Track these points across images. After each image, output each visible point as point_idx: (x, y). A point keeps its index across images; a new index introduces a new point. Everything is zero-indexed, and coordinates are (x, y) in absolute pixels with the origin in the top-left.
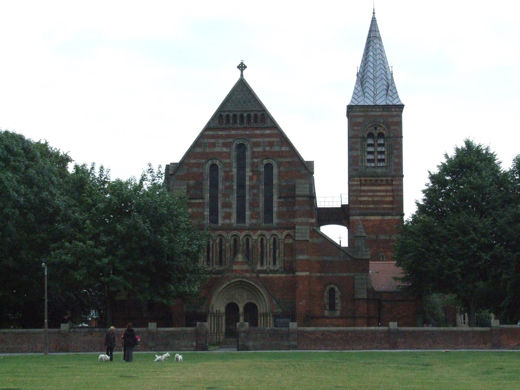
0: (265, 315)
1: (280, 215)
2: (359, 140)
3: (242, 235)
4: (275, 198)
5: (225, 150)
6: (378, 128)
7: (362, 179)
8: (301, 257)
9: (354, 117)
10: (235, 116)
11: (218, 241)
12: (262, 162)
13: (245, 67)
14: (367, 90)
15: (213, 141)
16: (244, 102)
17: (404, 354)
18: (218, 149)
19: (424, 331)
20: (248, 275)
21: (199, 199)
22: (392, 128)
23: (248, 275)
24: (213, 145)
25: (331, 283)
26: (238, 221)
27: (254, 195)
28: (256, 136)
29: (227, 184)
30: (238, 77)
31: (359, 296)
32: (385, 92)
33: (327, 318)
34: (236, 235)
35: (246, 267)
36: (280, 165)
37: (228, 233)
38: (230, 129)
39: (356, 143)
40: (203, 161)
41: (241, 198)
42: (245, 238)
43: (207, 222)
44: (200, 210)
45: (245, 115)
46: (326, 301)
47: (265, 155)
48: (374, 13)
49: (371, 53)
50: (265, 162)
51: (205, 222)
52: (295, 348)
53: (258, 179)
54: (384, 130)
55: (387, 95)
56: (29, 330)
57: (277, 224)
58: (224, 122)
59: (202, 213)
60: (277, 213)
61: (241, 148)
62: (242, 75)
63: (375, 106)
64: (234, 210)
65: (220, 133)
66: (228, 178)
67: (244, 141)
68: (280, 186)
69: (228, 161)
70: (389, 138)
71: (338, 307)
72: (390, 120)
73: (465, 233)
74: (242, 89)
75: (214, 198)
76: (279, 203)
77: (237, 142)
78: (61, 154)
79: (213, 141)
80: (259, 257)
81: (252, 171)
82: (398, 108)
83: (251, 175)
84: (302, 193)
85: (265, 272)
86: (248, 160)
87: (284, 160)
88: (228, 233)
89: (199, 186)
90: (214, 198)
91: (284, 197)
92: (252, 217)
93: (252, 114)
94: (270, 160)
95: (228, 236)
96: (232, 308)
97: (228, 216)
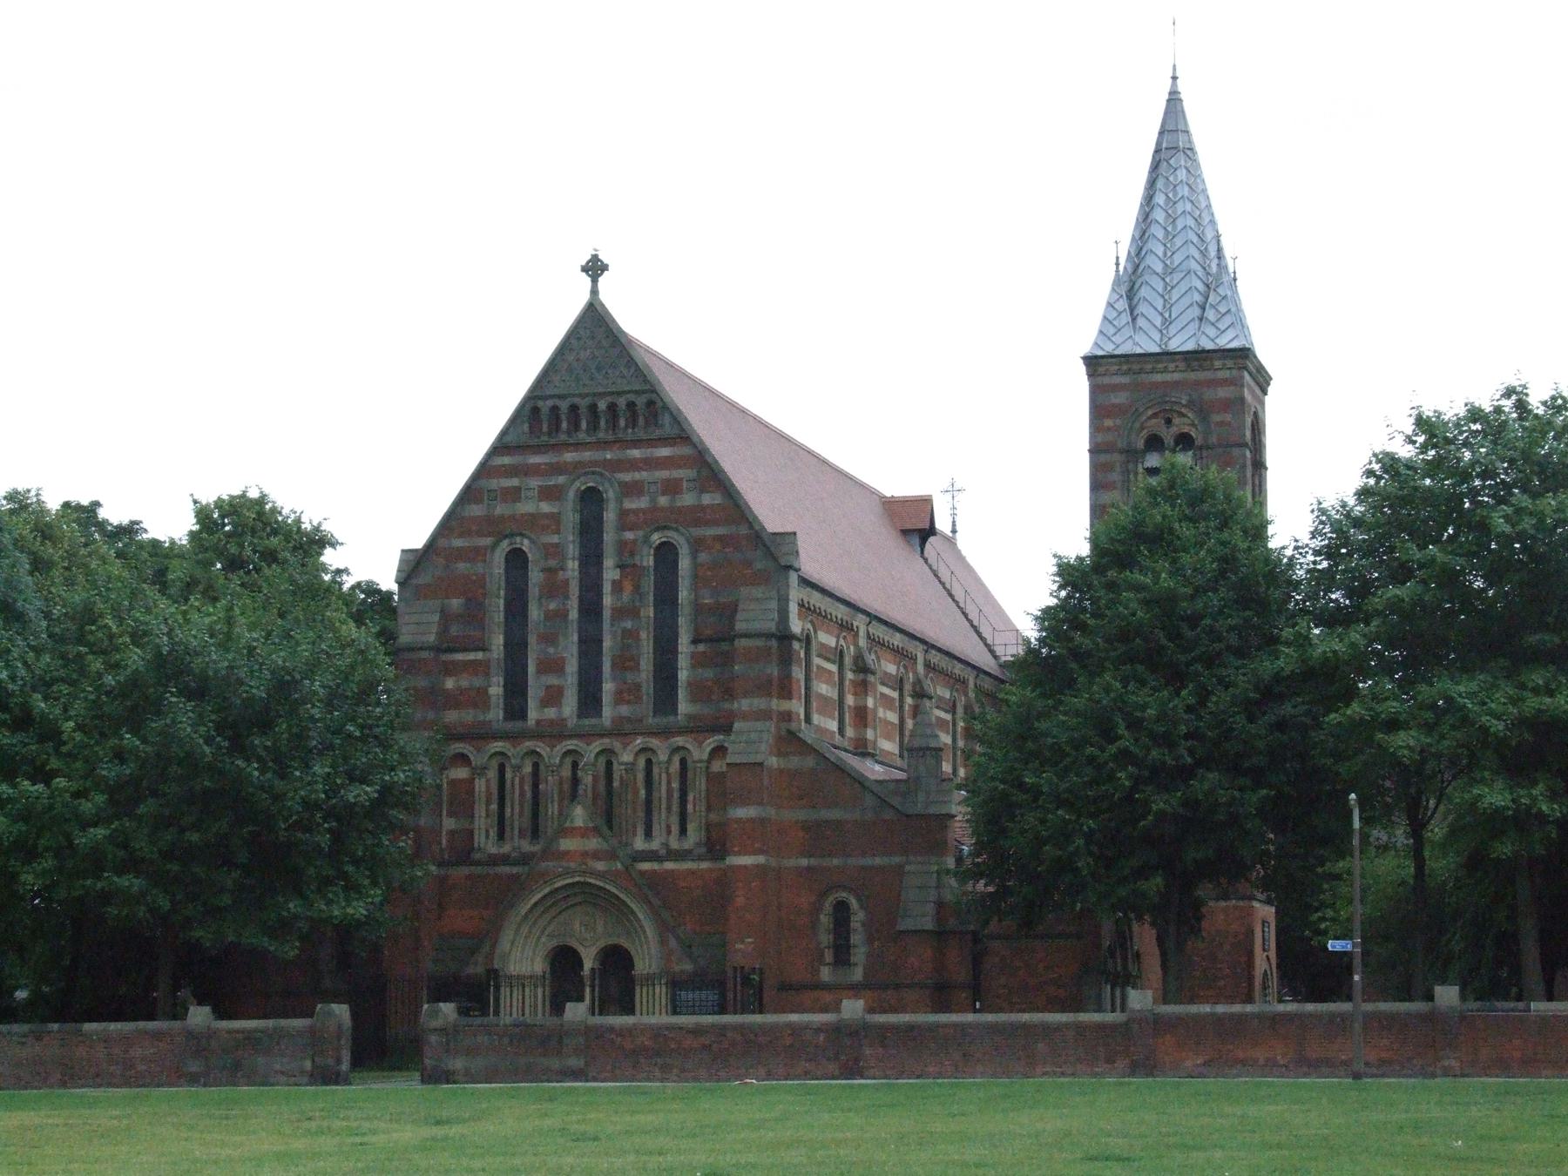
0: (650, 980)
1: (699, 691)
2: (1117, 457)
3: (591, 750)
5: (546, 507)
6: (1176, 421)
8: (742, 813)
10: (574, 408)
11: (528, 769)
12: (646, 539)
13: (604, 268)
14: (1142, 308)
15: (515, 482)
16: (599, 369)
17: (877, 1088)
18: (526, 507)
20: (600, 866)
22: (1216, 418)
23: (600, 866)
24: (514, 495)
28: (633, 465)
29: (552, 606)
30: (584, 298)
31: (906, 924)
32: (1197, 311)
34: (502, 754)
35: (593, 843)
36: (697, 545)
40: (488, 541)
42: (602, 760)
43: (496, 714)
44: (478, 682)
45: (602, 405)
46: (825, 939)
47: (655, 520)
48: (1174, 78)
49: (1160, 199)
50: (656, 538)
51: (491, 716)
52: (577, 1075)
54: (1193, 425)
55: (1201, 319)
56: (283, 1022)
57: (690, 717)
58: (545, 429)
59: (483, 692)
60: (689, 684)
61: (591, 499)
62: (594, 292)
63: (1167, 355)
66: (554, 589)
68: (698, 608)
69: (555, 539)
70: (1208, 448)
71: (859, 954)
72: (1209, 394)
73: (1109, 735)
74: (595, 333)
75: (516, 649)
76: (693, 656)
77: (581, 484)
78: (306, 526)
79: (515, 482)
80: (641, 814)
81: (621, 567)
82: (1127, 362)
83: (617, 577)
84: (756, 626)
85: (652, 856)
86: (609, 537)
87: (711, 532)
89: (475, 613)
90: (516, 649)
91: (710, 640)
92: (619, 698)
93: (621, 402)
94: (671, 533)
95: (552, 754)
96: (564, 960)
97: (554, 699)
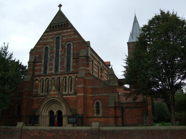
1: (74, 67)
4: (72, 60)
5: (51, 40)
9: (129, 46)
13: (62, 6)
15: (47, 37)
18: (48, 41)
19: (123, 131)
21: (40, 63)
23: (56, 96)
24: (47, 39)
25: (97, 99)
26: (55, 72)
28: (64, 33)
31: (110, 106)
33: (95, 117)
35: (56, 92)
36: (74, 44)
37: (50, 77)
38: (53, 31)
41: (57, 61)
44: (40, 68)
46: (95, 109)
48: (135, 15)
49: (135, 26)
50: (68, 43)
53: (64, 52)
60: (72, 66)
62: (60, 9)
64: (54, 66)
65: (50, 33)
66: (52, 52)
67: (59, 35)
74: (60, 15)
75: (46, 62)
76: (73, 61)
86: (60, 44)
87: (76, 42)
88: (50, 77)
89: (40, 57)
90: (46, 62)
92: (61, 69)
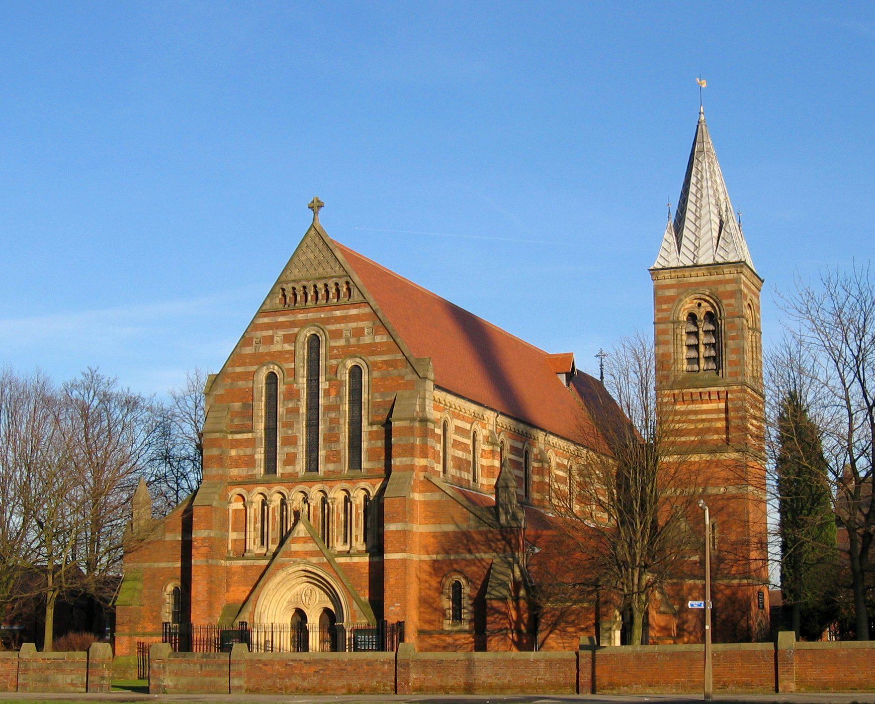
5: (288, 347)
7: (676, 392)
15: (270, 333)
18: (277, 347)
23: (314, 560)
26: (308, 469)
27: (332, 421)
35: (311, 547)
36: (371, 367)
39: (665, 332)
40: (254, 368)
44: (248, 451)
57: (368, 470)
65: (281, 319)
72: (721, 289)
76: (370, 433)
87: (378, 359)
89: (248, 412)
92: (328, 460)
